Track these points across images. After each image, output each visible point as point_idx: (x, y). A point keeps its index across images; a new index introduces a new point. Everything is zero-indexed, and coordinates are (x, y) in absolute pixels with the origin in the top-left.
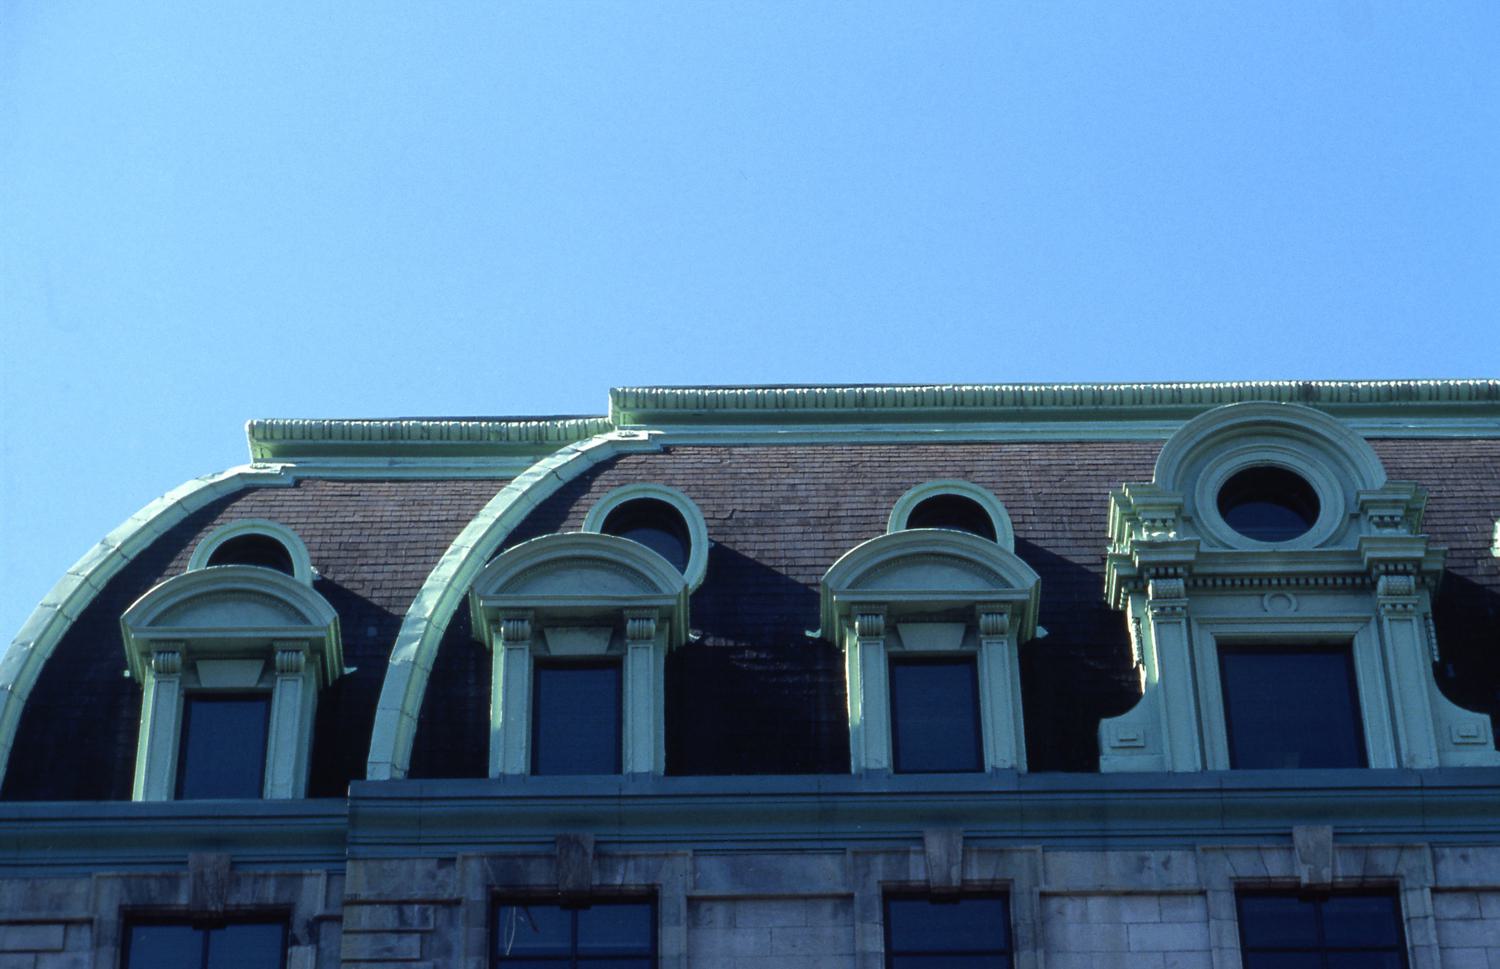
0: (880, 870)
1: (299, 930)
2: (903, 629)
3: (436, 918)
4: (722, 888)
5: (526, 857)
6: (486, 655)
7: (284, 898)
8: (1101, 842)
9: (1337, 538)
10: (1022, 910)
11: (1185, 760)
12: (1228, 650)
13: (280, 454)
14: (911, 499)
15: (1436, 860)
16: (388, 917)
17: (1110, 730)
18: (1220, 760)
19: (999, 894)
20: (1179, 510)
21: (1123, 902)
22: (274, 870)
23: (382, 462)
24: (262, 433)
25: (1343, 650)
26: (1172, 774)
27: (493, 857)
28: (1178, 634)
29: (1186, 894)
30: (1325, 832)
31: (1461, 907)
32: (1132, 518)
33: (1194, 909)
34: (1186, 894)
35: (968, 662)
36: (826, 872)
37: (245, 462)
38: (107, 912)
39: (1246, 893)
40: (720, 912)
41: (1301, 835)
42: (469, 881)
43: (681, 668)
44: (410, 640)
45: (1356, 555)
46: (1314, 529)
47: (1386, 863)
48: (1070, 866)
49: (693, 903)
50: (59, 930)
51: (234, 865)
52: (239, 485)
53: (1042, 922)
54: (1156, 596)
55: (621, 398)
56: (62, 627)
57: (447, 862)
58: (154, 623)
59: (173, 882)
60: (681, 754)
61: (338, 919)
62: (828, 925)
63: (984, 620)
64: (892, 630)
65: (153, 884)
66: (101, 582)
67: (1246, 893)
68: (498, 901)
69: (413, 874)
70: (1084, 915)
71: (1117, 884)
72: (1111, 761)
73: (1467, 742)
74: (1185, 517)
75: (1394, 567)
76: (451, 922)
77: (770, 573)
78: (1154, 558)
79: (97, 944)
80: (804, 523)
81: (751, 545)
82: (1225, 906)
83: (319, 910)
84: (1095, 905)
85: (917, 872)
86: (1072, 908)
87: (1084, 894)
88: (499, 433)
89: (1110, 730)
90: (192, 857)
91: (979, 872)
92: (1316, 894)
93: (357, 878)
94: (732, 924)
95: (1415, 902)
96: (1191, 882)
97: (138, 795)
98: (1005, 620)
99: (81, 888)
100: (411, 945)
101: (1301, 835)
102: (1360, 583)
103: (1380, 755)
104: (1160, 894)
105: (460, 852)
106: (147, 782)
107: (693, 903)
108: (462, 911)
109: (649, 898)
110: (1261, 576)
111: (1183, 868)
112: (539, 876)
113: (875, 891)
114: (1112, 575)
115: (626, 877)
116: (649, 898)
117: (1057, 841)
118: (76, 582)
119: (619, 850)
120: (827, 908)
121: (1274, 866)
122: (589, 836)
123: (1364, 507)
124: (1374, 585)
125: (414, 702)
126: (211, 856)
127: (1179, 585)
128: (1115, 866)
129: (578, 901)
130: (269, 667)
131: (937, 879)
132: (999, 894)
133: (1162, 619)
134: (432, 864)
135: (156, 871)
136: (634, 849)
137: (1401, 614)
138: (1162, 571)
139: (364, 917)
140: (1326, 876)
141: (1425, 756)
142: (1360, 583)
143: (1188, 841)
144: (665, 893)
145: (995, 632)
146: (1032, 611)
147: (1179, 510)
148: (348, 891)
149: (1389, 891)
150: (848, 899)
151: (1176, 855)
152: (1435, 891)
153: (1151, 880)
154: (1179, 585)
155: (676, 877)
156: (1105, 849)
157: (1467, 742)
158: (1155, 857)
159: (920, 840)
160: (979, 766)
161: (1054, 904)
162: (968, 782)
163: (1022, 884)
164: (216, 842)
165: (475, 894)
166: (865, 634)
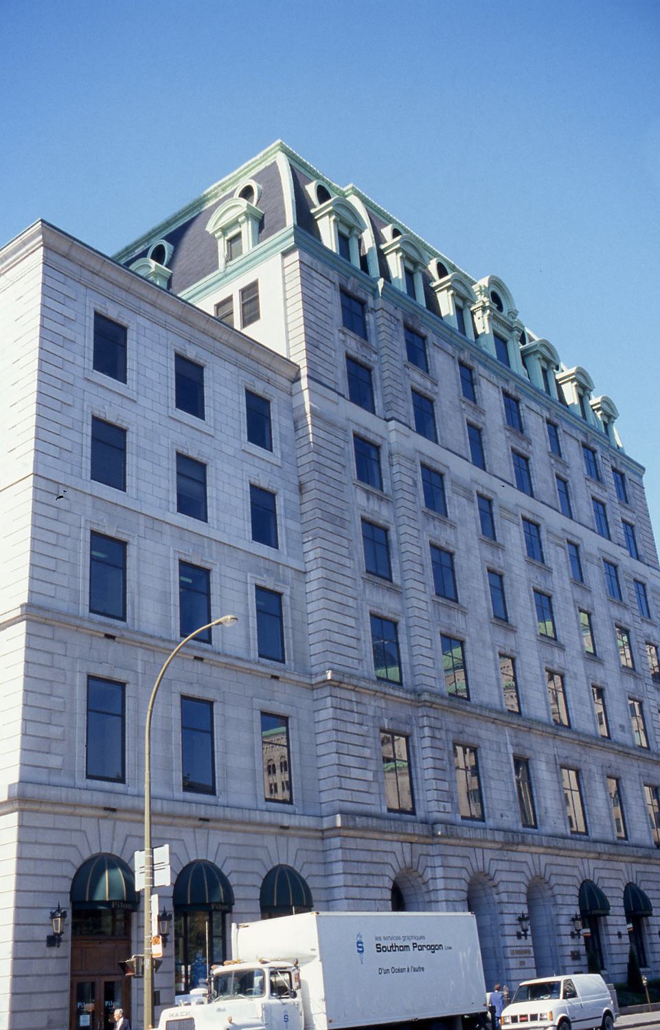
54: (489, 315)
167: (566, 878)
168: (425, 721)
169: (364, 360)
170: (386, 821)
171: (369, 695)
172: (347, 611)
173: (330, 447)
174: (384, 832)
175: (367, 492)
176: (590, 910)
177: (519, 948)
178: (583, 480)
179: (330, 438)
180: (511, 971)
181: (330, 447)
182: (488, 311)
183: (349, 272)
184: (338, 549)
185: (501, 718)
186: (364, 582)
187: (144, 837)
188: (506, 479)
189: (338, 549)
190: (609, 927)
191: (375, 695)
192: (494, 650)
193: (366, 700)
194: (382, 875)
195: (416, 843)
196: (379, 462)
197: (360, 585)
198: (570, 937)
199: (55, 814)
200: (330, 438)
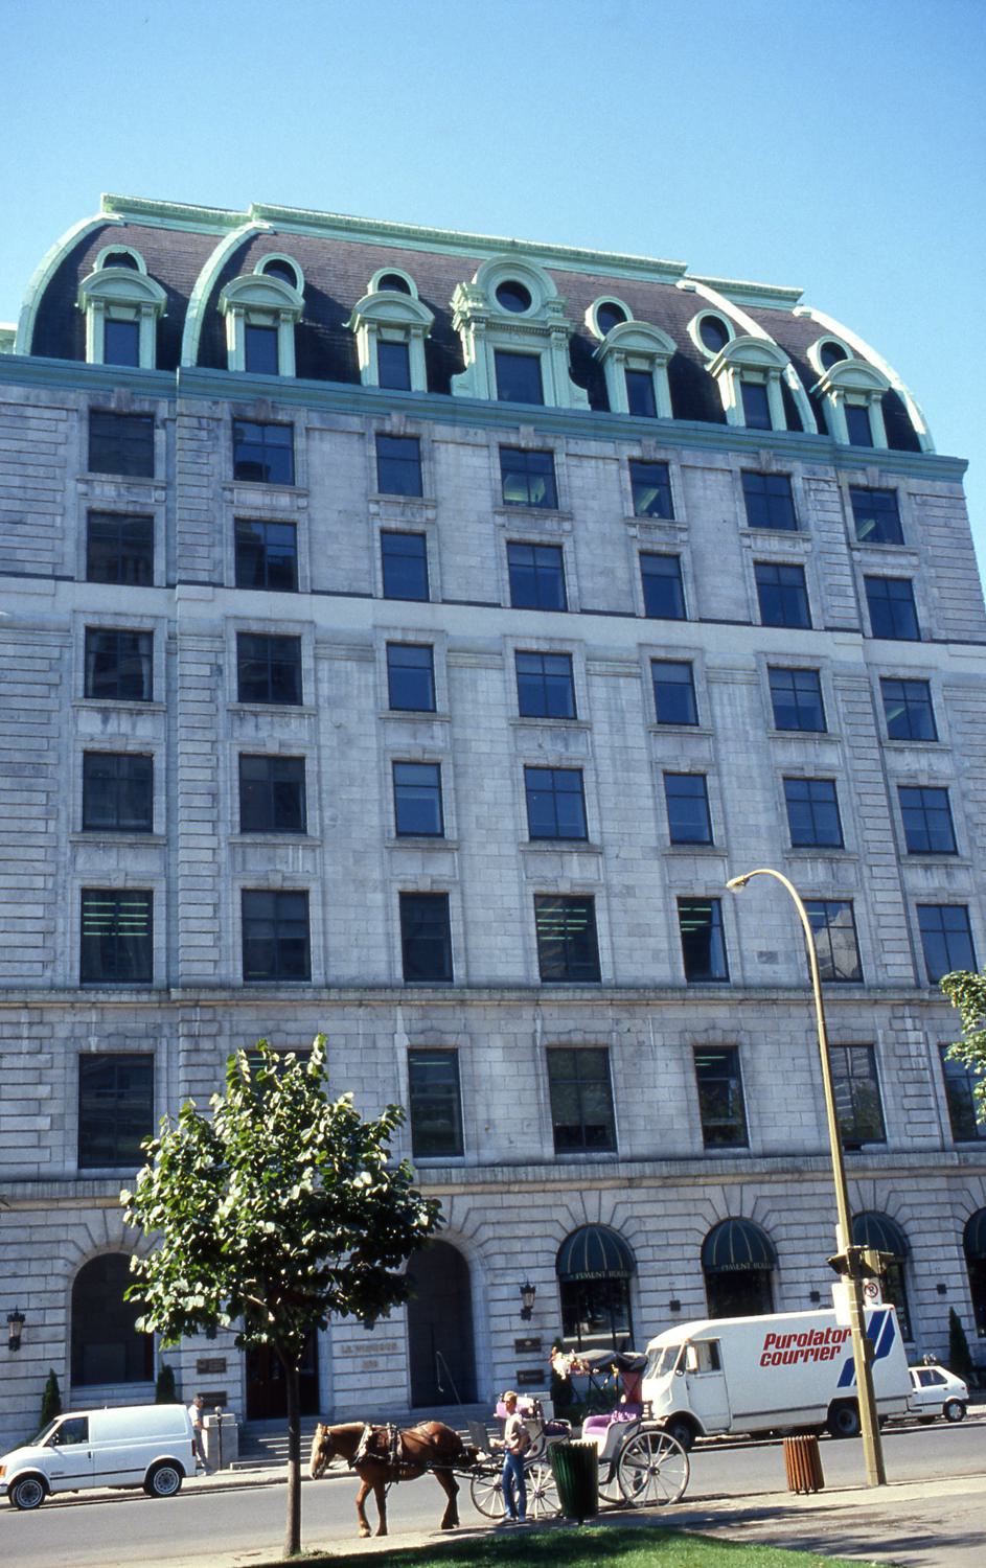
0: (375, 425)
1: (159, 423)
2: (383, 330)
3: (213, 424)
4: (318, 426)
5: (247, 405)
6: (223, 319)
7: (152, 409)
8: (453, 423)
9: (537, 315)
10: (424, 446)
11: (484, 396)
12: (499, 353)
13: (117, 209)
14: (379, 274)
15: (567, 443)
16: (194, 422)
17: (456, 379)
18: (495, 397)
19: (416, 439)
20: (483, 295)
21: (461, 448)
22: (148, 398)
23: (158, 220)
24: (109, 200)
25: (536, 358)
26: (479, 400)
27: (233, 403)
28: (481, 345)
29: (482, 446)
30: (531, 429)
31: (573, 461)
32: (465, 295)
33: (485, 452)
34: (482, 446)
35: (136, 325)
36: (355, 423)
37: (104, 214)
38: (84, 406)
39: (503, 448)
40: (317, 433)
41: (523, 429)
42: (224, 411)
43: (300, 333)
44: (193, 308)
45: (545, 322)
46: (527, 312)
47: (551, 442)
48: (442, 431)
49: (307, 429)
50: (64, 412)
51: (133, 394)
52: (102, 224)
53: (432, 451)
54: (476, 329)
55: (256, 208)
56: (46, 281)
57: (216, 403)
58: (93, 288)
59: (108, 398)
60: (302, 370)
61: (175, 420)
62: (356, 444)
63: (413, 331)
64: (379, 330)
65: (101, 398)
66: (59, 262)
67: (503, 448)
68: (238, 420)
69: (203, 406)
70: (447, 450)
71: (459, 440)
72: (456, 392)
73: (579, 400)
74: (485, 300)
75: (559, 330)
76: (218, 427)
77: (326, 296)
78: (475, 314)
79: (81, 419)
80: (335, 276)
81: (319, 284)
82: (496, 452)
83: (166, 416)
84: (451, 446)
85: (388, 428)
86: (443, 447)
87: (447, 442)
88: (205, 213)
89: (456, 379)
90: (116, 389)
91: (411, 430)
92: (524, 451)
93: (181, 405)
94: (321, 439)
95: (559, 458)
96: (484, 442)
97: (90, 359)
98: (290, 317)
99: (72, 396)
100: (204, 434)
101: (523, 429)
102: (545, 333)
103: (549, 401)
104: (474, 445)
105: (221, 400)
106: (93, 354)
107: (307, 429)
108: (222, 423)
109: (291, 425)
110: (508, 325)
111: (481, 436)
112: (250, 413)
113: (373, 433)
114: (457, 320)
115: (282, 417)
116: (291, 425)
117: (437, 421)
118: (50, 261)
119: (280, 406)
120: (356, 437)
121: (513, 440)
122: (269, 399)
123: (548, 303)
124: (549, 335)
125: (197, 335)
126: (123, 390)
127: (483, 326)
128: (456, 432)
129: (263, 424)
130: (138, 312)
131: (395, 431)
132: (416, 439)
133: (477, 337)
134: (210, 403)
135: (101, 393)
136: (285, 406)
137: (559, 347)
138: (477, 320)
139: (186, 421)
140: (531, 445)
141: (565, 405)
142: (545, 333)
143: (484, 426)
144: (297, 425)
145: (285, 321)
146: (300, 314)
147: (483, 295)
148: (178, 410)
149: (550, 453)
150: (363, 434)
151: (480, 431)
152: (567, 455)
153: (470, 439)
154: (483, 326)
155: (302, 418)
156: (454, 426)
157: (579, 400)
158: (472, 431)
159: (389, 414)
160: (409, 389)
161: (436, 444)
162: (403, 394)
163: (425, 436)
164: (124, 384)
165: (227, 417)
166: (237, 315)
167: (523, 1226)
168: (182, 1029)
169: (131, 508)
170: (573, 1167)
171: (63, 1008)
172: (29, 896)
173: (27, 664)
174: (58, 1200)
175: (130, 712)
176: (719, 1265)
177: (366, 1343)
178: (734, 538)
179: (29, 651)
180: (336, 1378)
181: (27, 664)
182: (473, 325)
183: (754, 444)
184: (22, 811)
185: (377, 997)
186: (390, 853)
187: (834, 1194)
188: (473, 599)
189: (22, 811)
190: (918, 1279)
191: (73, 1008)
192: (385, 891)
193: (49, 1017)
194: (52, 1258)
195: (586, 1190)
196: (150, 657)
197: (65, 854)
198: (6, 1347)
199: (473, 1194)
200: (29, 651)
